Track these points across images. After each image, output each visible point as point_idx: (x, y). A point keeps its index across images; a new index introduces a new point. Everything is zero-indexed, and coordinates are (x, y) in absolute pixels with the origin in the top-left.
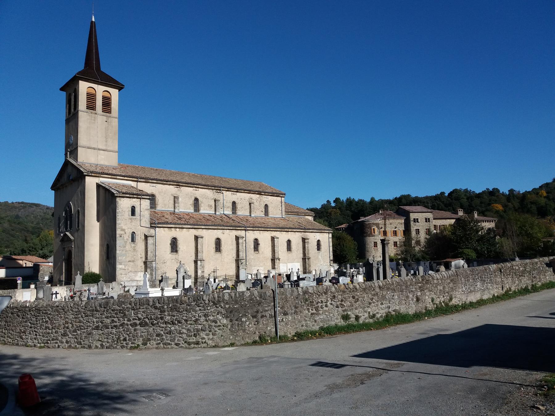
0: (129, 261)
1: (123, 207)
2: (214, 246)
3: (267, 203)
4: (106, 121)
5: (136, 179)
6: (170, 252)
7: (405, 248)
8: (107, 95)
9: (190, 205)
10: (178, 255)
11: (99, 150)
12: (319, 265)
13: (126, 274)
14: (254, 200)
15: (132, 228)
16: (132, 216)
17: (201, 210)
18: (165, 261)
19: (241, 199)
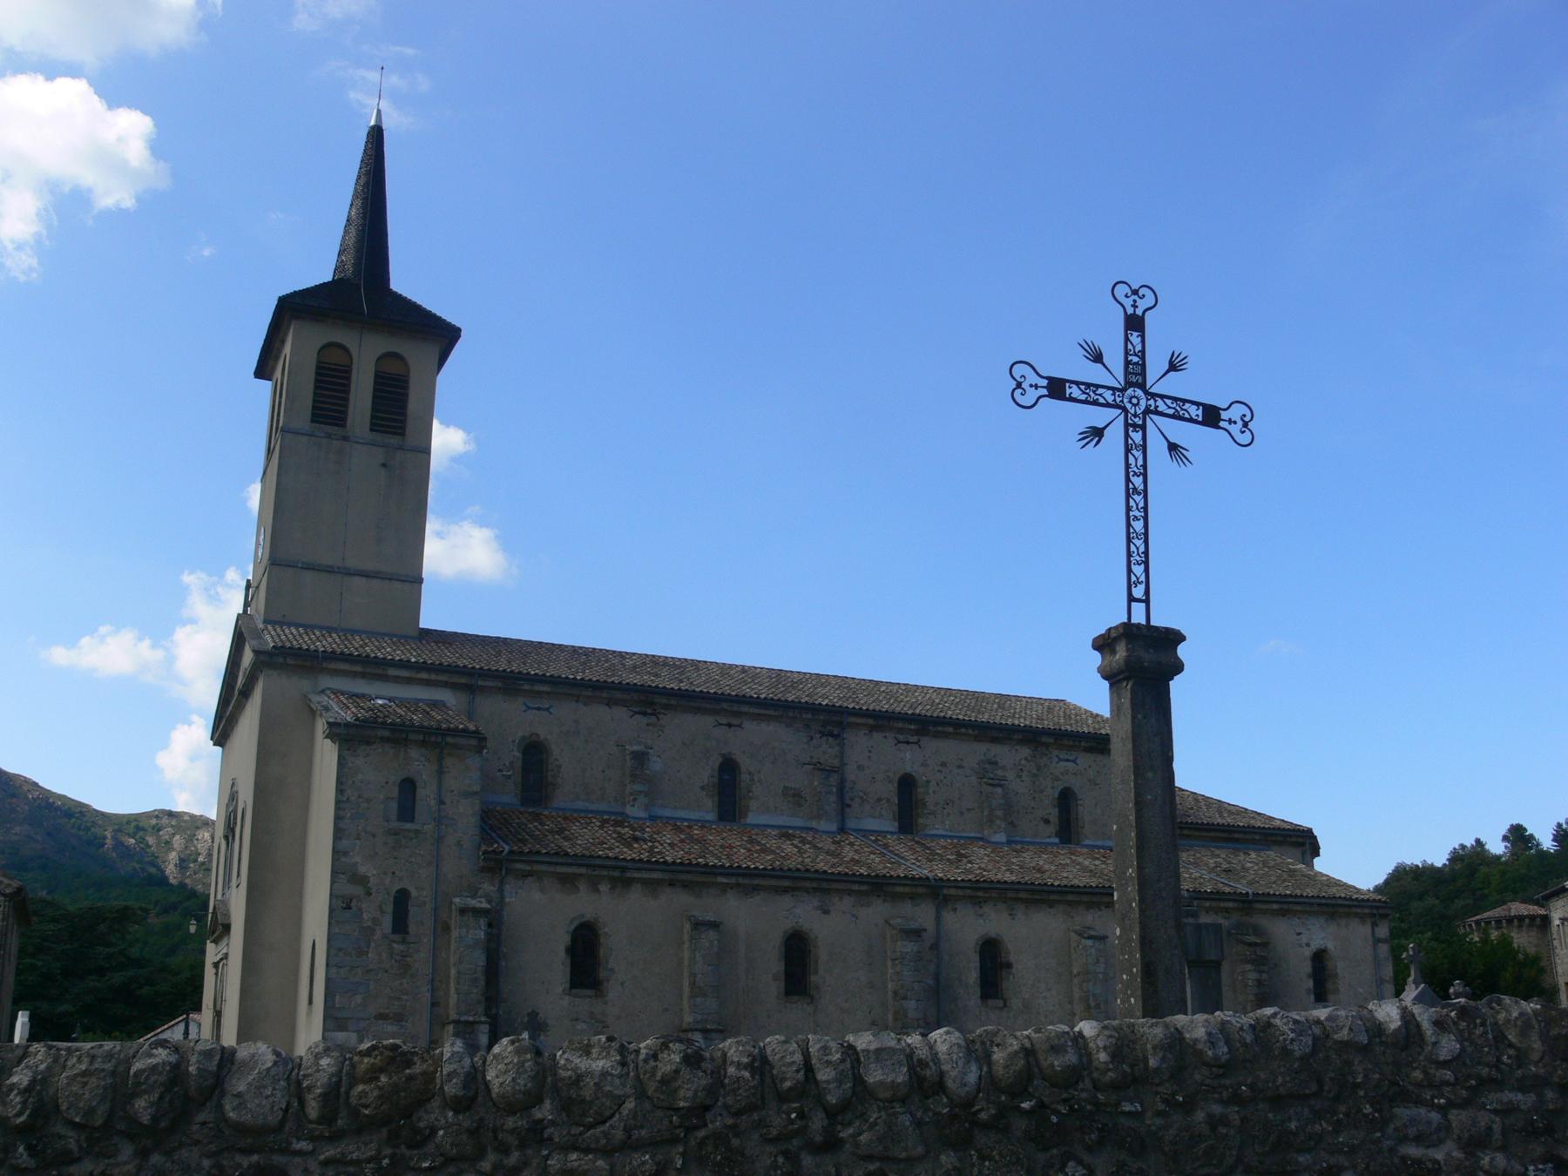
0: (381, 1017)
4: (384, 465)
5: (463, 680)
6: (568, 986)
7: (13, 1161)
10: (606, 1003)
14: (1004, 768)
17: (750, 815)
19: (944, 764)
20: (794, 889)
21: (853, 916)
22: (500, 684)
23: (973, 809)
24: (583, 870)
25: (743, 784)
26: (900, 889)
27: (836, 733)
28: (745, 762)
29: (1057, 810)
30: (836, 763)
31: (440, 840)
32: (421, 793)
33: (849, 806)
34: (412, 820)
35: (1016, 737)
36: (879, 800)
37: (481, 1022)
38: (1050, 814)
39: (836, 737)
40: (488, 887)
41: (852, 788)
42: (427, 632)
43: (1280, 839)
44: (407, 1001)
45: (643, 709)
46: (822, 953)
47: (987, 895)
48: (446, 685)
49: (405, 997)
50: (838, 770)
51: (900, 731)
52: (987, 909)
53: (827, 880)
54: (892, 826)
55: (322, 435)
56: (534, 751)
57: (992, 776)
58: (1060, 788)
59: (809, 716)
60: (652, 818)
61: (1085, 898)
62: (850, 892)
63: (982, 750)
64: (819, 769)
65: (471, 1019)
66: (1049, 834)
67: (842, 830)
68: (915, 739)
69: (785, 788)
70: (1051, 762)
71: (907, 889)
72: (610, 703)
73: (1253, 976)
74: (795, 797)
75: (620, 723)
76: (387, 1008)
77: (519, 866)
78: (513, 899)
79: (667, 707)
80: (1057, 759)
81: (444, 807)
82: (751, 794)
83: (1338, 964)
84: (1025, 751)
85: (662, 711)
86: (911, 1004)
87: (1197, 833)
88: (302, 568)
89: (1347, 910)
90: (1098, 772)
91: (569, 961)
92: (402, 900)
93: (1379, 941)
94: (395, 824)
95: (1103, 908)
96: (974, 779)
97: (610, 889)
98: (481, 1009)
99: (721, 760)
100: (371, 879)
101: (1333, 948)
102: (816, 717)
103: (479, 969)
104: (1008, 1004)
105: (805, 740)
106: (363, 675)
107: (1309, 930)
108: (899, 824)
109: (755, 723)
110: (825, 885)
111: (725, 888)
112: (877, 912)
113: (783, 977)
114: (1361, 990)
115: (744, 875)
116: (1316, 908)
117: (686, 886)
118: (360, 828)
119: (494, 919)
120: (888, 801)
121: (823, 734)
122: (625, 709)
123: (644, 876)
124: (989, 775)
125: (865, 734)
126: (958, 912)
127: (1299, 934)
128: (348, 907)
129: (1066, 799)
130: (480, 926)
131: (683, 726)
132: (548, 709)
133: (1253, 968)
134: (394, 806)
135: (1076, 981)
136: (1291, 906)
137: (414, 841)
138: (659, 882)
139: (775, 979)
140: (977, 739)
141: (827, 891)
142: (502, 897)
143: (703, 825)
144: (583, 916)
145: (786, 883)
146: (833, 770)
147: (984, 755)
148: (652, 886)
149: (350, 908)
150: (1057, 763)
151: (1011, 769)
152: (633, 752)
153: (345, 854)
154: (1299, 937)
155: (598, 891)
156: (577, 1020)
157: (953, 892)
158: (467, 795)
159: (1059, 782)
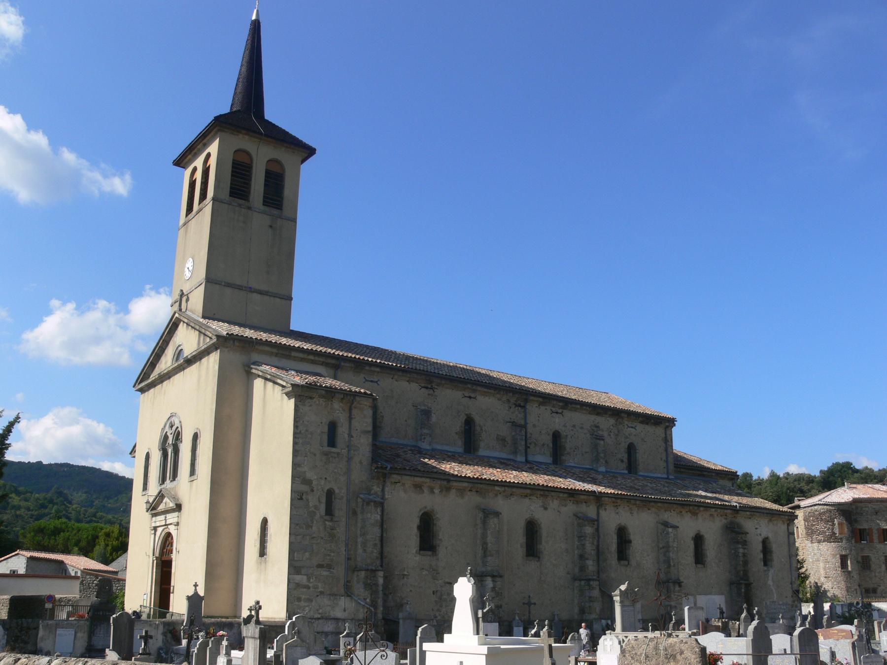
0: (320, 566)
11: (251, 290)
12: (768, 603)
13: (310, 600)
14: (602, 430)
15: (329, 479)
16: (328, 446)
17: (480, 450)
18: (404, 571)
19: (574, 426)
23: (588, 452)
28: (477, 419)
30: (523, 422)
31: (349, 459)
36: (543, 445)
38: (623, 457)
41: (530, 437)
42: (292, 331)
44: (333, 556)
45: (426, 385)
48: (323, 364)
49: (333, 554)
50: (524, 426)
53: (548, 491)
54: (549, 460)
58: (628, 443)
68: (560, 411)
70: (624, 428)
76: (323, 561)
78: (390, 496)
80: (626, 427)
81: (352, 439)
84: (612, 421)
87: (687, 471)
88: (224, 285)
91: (418, 534)
92: (330, 495)
94: (326, 449)
97: (440, 492)
100: (314, 482)
104: (630, 563)
106: (276, 355)
109: (483, 397)
113: (525, 546)
118: (307, 450)
120: (548, 445)
122: (417, 384)
126: (607, 511)
127: (756, 529)
128: (301, 499)
130: (378, 513)
131: (448, 396)
132: (377, 382)
134: (325, 437)
137: (337, 459)
142: (383, 495)
146: (520, 426)
148: (461, 492)
150: (627, 428)
151: (606, 431)
153: (299, 466)
156: (423, 569)
159: (628, 439)
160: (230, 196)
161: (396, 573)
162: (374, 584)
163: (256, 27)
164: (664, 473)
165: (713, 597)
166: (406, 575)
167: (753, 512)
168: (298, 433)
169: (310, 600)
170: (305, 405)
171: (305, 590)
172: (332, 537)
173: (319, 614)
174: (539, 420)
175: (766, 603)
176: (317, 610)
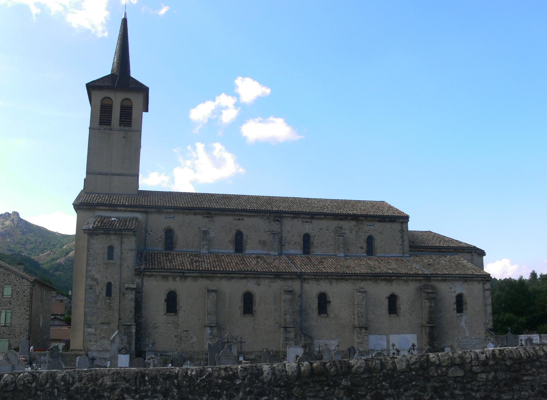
0: (102, 323)
1: (95, 248)
2: (241, 304)
3: (371, 233)
4: (124, 137)
5: (143, 210)
6: (166, 312)
8: (127, 103)
9: (229, 242)
10: (179, 318)
12: (460, 338)
13: (96, 341)
14: (345, 229)
17: (247, 250)
19: (321, 229)
20: (247, 277)
21: (269, 286)
22: (156, 210)
24: (169, 274)
25: (244, 240)
26: (286, 276)
27: (279, 220)
28: (245, 232)
29: (366, 244)
30: (279, 230)
31: (121, 265)
32: (115, 250)
33: (284, 245)
34: (112, 259)
35: (349, 218)
36: (296, 243)
37: (132, 325)
39: (279, 221)
40: (138, 280)
43: (462, 251)
45: (207, 216)
46: (257, 299)
47: (321, 277)
48: (138, 212)
49: (110, 317)
51: (303, 218)
52: (321, 282)
54: (301, 252)
55: (103, 129)
56: (169, 233)
57: (340, 232)
58: (367, 236)
59: (268, 215)
60: (210, 253)
61: (359, 277)
62: (268, 278)
63: (336, 223)
64: (272, 233)
65: (130, 324)
66: (362, 253)
67: (280, 254)
68: (310, 220)
69: (260, 241)
71: (289, 276)
72: (195, 214)
73: (428, 304)
74: (263, 243)
75: (200, 221)
77: (147, 273)
79: (216, 214)
81: (122, 254)
82: (247, 243)
83: (467, 299)
84: (354, 223)
85: (214, 216)
86: (288, 317)
87: (426, 250)
89: (471, 279)
90: (383, 229)
92: (109, 286)
93: (486, 290)
94: (107, 261)
95: (368, 281)
96: (333, 234)
97: (180, 279)
98: (133, 320)
99: (236, 231)
100: (99, 279)
101: (465, 293)
102: (271, 215)
103: (132, 307)
104: (329, 316)
105: (267, 223)
106: (110, 210)
107: (455, 286)
108: (303, 251)
109: (249, 218)
110: (257, 276)
111: (221, 278)
112: (278, 284)
114: (477, 308)
115: (227, 273)
116: (457, 279)
117: (207, 277)
118: (95, 263)
119: (139, 292)
121: (274, 221)
123: (191, 275)
124: (339, 232)
125: (290, 220)
129: (370, 240)
131: (222, 221)
132: (173, 218)
133: (428, 301)
134: (106, 255)
135: (356, 307)
136: (447, 278)
138: (197, 277)
139: (239, 308)
140: (334, 219)
141: (259, 278)
142: (143, 283)
143: (228, 255)
144: (170, 289)
145: (243, 276)
147: (337, 225)
149: (92, 289)
152: (203, 231)
153: (90, 271)
154: (451, 289)
155: (176, 280)
156: (168, 323)
157: (307, 277)
158: (131, 250)
159: (367, 234)
160: (100, 124)
161: (151, 326)
162: (130, 332)
163: (125, 22)
164: (400, 253)
165: (406, 335)
166: (157, 327)
167: (447, 277)
168: (89, 254)
169: (96, 341)
170: (93, 239)
171: (94, 336)
172: (110, 308)
173: (102, 348)
174: (292, 228)
175: (458, 339)
176: (101, 346)
